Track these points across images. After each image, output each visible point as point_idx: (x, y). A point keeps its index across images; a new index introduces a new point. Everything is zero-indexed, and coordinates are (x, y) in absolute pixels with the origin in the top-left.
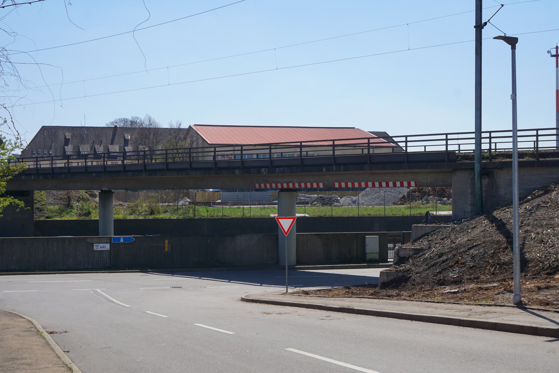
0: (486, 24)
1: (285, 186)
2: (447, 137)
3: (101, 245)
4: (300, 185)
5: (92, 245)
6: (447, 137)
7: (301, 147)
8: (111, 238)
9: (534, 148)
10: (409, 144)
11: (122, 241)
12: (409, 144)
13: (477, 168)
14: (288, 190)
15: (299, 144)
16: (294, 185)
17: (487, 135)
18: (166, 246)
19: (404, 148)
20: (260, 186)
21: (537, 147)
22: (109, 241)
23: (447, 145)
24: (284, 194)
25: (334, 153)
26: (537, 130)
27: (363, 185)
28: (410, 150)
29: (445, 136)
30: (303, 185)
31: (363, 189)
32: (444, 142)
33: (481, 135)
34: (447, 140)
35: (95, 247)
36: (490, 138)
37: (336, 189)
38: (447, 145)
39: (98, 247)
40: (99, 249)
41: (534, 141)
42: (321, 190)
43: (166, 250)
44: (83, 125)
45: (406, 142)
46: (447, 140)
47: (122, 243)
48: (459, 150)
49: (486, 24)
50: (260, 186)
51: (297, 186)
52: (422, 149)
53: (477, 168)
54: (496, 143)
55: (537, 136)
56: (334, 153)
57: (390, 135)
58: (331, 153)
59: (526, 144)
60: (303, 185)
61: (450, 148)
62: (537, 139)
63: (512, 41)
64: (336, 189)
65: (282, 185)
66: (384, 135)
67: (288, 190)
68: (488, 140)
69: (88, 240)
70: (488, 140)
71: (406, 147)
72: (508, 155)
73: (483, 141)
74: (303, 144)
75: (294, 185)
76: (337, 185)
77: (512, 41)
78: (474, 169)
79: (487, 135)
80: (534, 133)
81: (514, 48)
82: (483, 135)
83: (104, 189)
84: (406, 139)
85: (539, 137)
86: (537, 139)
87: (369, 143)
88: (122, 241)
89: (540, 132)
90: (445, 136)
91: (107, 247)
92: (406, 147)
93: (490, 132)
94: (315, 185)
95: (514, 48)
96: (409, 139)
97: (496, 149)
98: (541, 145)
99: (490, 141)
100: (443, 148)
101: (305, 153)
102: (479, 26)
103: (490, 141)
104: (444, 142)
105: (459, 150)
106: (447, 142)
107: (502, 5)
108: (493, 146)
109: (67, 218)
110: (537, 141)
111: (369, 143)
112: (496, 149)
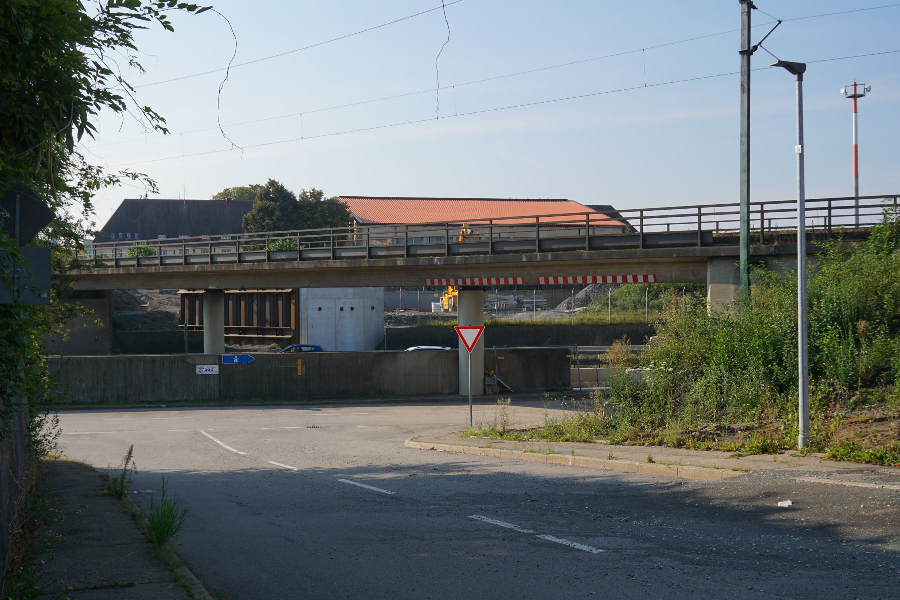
0: (756, 48)
1: (469, 282)
2: (762, 208)
3: (206, 367)
4: (489, 281)
5: (194, 366)
6: (762, 208)
7: (492, 227)
8: (220, 357)
9: (825, 226)
10: (645, 222)
11: (236, 361)
12: (834, 212)
13: (743, 254)
14: (473, 288)
15: (489, 222)
16: (481, 281)
17: (759, 208)
18: (300, 368)
19: (638, 229)
20: (433, 282)
21: (830, 226)
22: (217, 362)
23: (700, 223)
24: (467, 294)
25: (700, 227)
26: (642, 211)
27: (580, 281)
28: (647, 230)
29: (760, 206)
30: (494, 282)
31: (581, 287)
32: (853, 212)
33: (749, 208)
34: (700, 215)
35: (198, 370)
36: (762, 212)
37: (541, 287)
38: (700, 223)
39: (203, 370)
40: (204, 373)
41: (826, 217)
42: (520, 288)
43: (300, 374)
44: (182, 198)
45: (642, 218)
46: (700, 215)
47: (237, 365)
48: (718, 230)
49: (756, 48)
50: (433, 282)
51: (485, 282)
52: (664, 229)
53: (743, 254)
54: (770, 220)
55: (830, 209)
56: (700, 227)
57: (617, 209)
58: (853, 221)
59: (816, 221)
60: (494, 282)
61: (705, 227)
62: (830, 213)
63: (797, 69)
64: (541, 287)
65: (464, 281)
66: (609, 211)
67: (473, 288)
68: (759, 216)
69: (188, 360)
70: (759, 216)
71: (642, 226)
72: (732, 240)
73: (752, 216)
74: (494, 222)
75: (481, 281)
76: (542, 281)
77: (797, 69)
78: (739, 257)
79: (759, 208)
80: (696, 211)
81: (800, 79)
82: (752, 208)
83: (210, 288)
84: (830, 204)
85: (751, 215)
86: (830, 213)
87: (588, 221)
88: (236, 361)
89: (703, 211)
90: (760, 206)
91: (216, 369)
92: (642, 226)
93: (762, 204)
94: (511, 282)
95: (800, 79)
96: (834, 204)
97: (770, 228)
98: (835, 221)
99: (762, 216)
100: (695, 228)
101: (498, 236)
102: (748, 53)
103: (762, 216)
104: (696, 219)
105: (718, 230)
106: (700, 219)
107: (780, 22)
108: (766, 225)
109: (566, 301)
110: (830, 216)
111: (588, 221)
112: (770, 228)
